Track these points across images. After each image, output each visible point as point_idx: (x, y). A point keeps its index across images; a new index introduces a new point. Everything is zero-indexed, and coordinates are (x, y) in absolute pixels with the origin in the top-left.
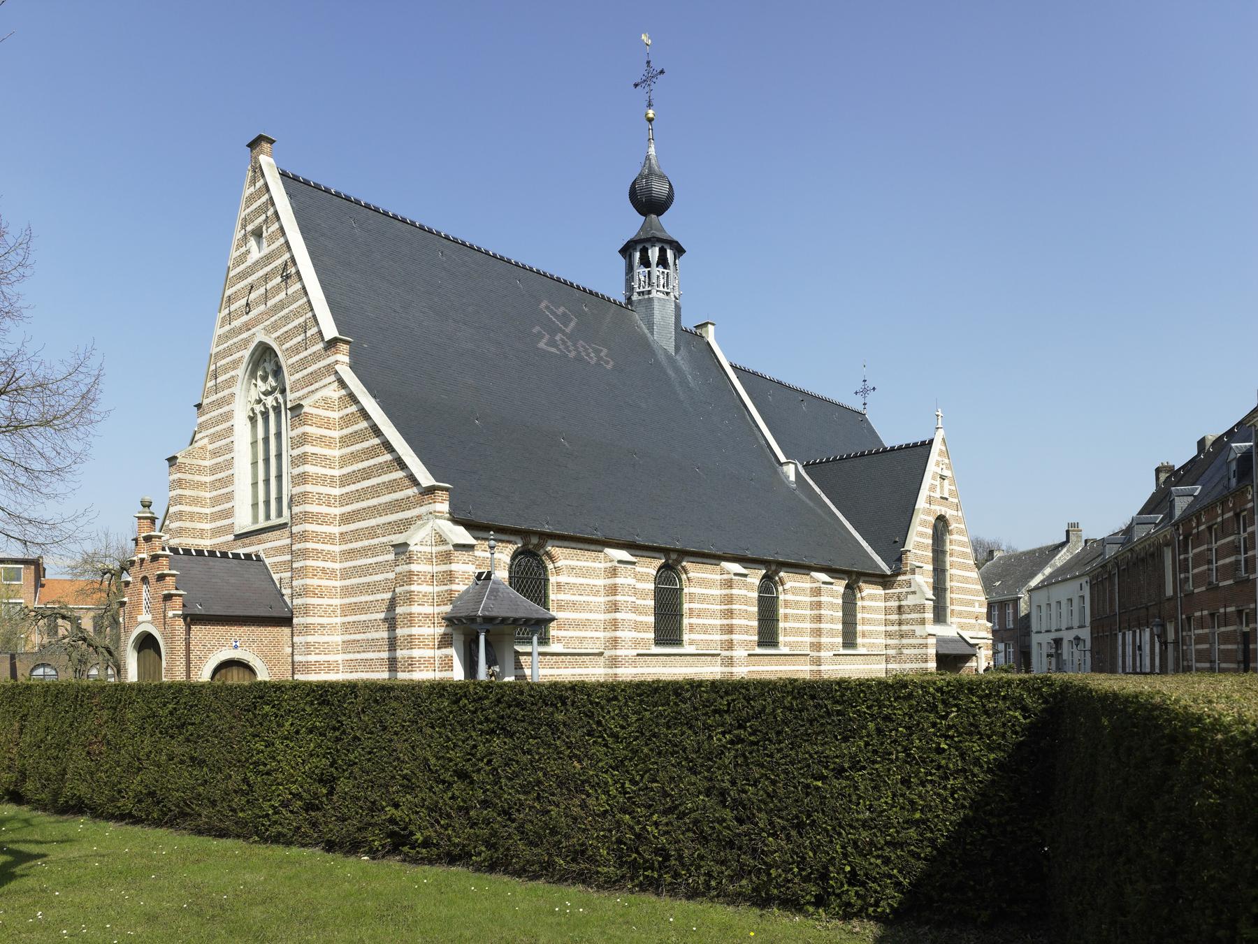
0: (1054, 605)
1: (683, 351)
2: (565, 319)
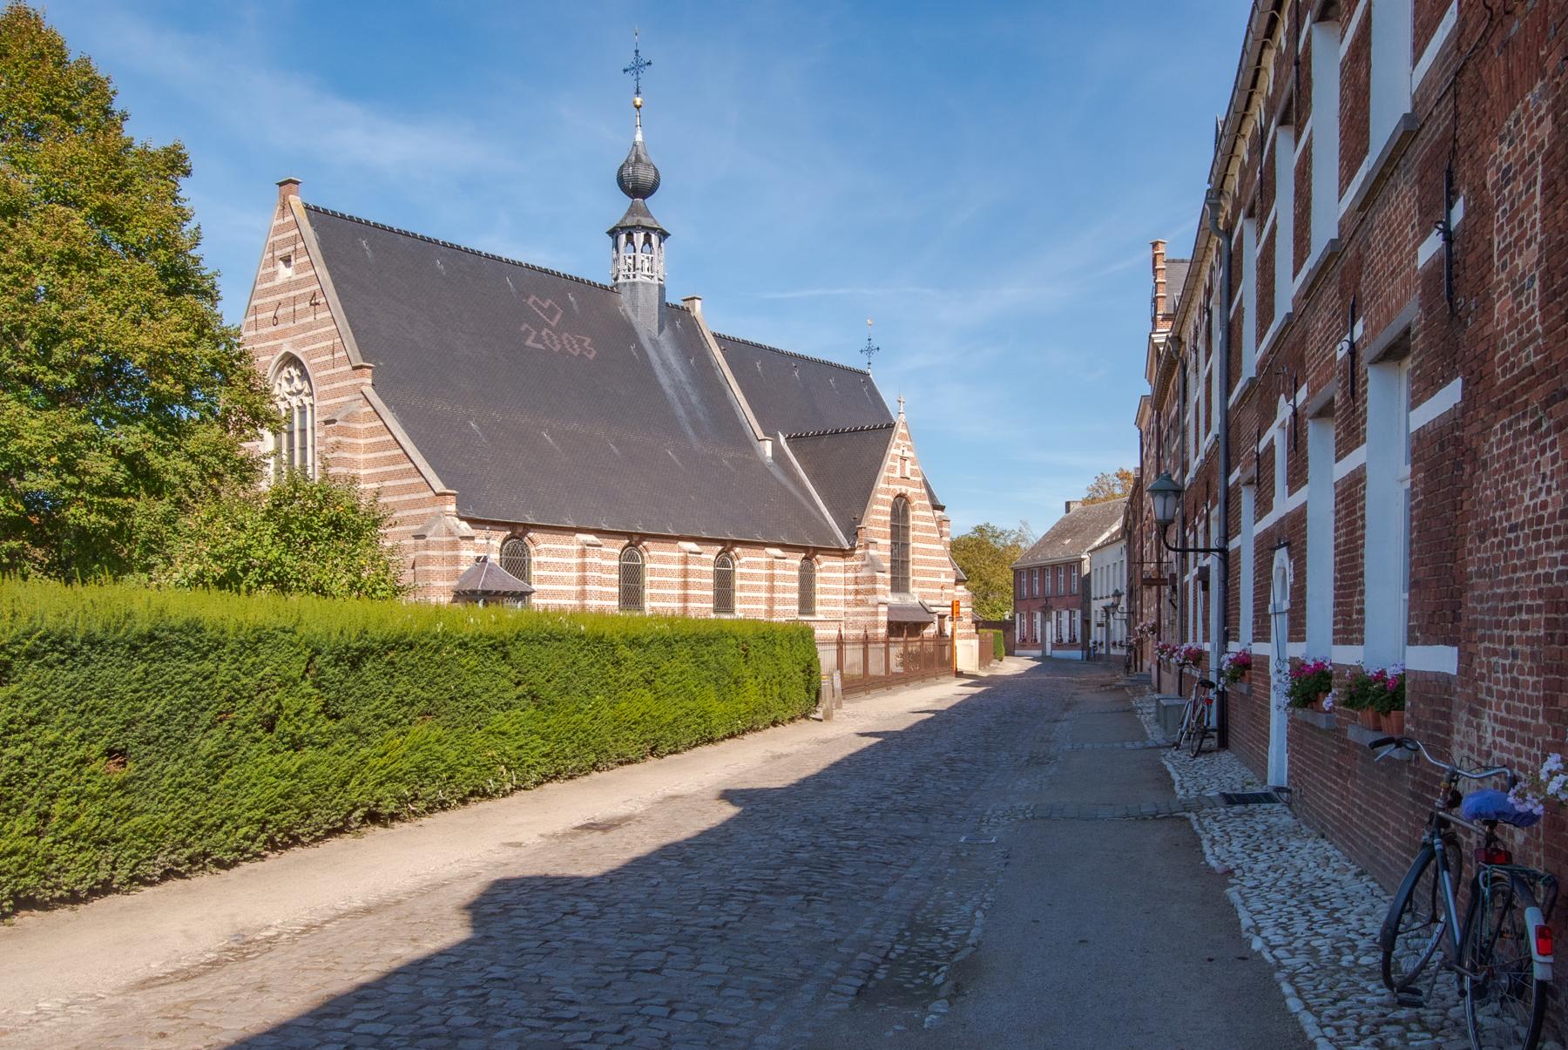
1: (667, 330)
2: (551, 312)
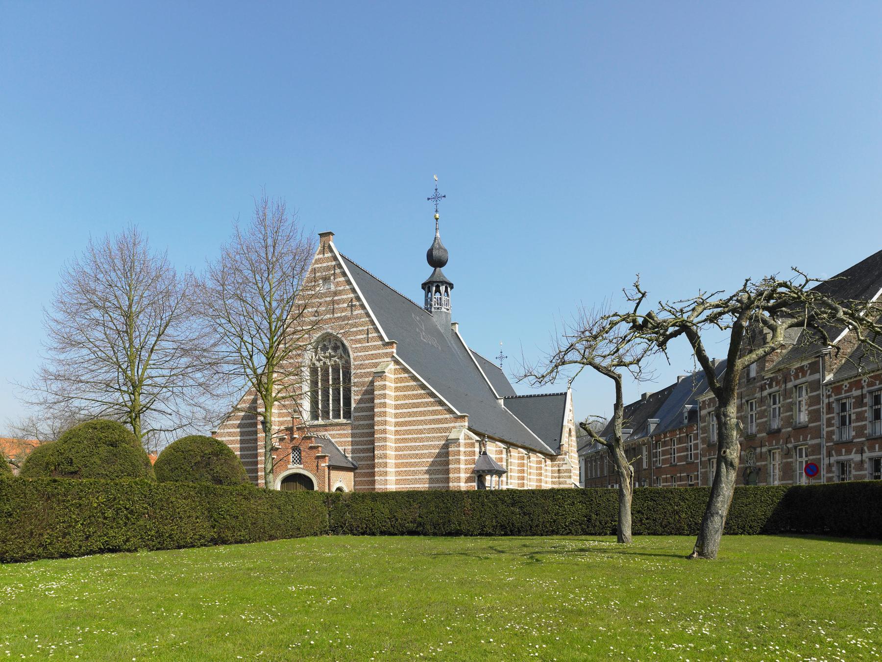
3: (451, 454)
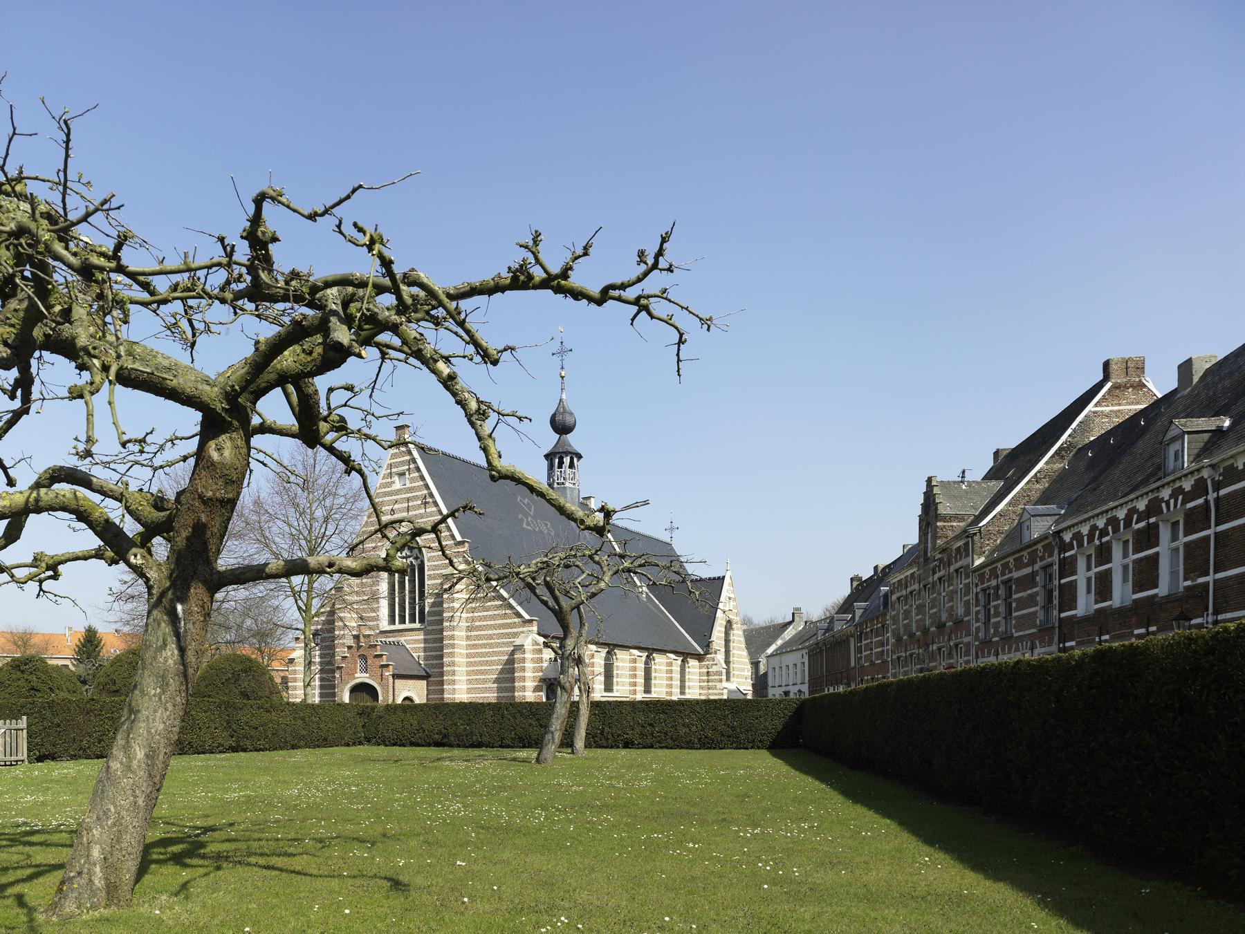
0: (784, 668)
3: (516, 661)
